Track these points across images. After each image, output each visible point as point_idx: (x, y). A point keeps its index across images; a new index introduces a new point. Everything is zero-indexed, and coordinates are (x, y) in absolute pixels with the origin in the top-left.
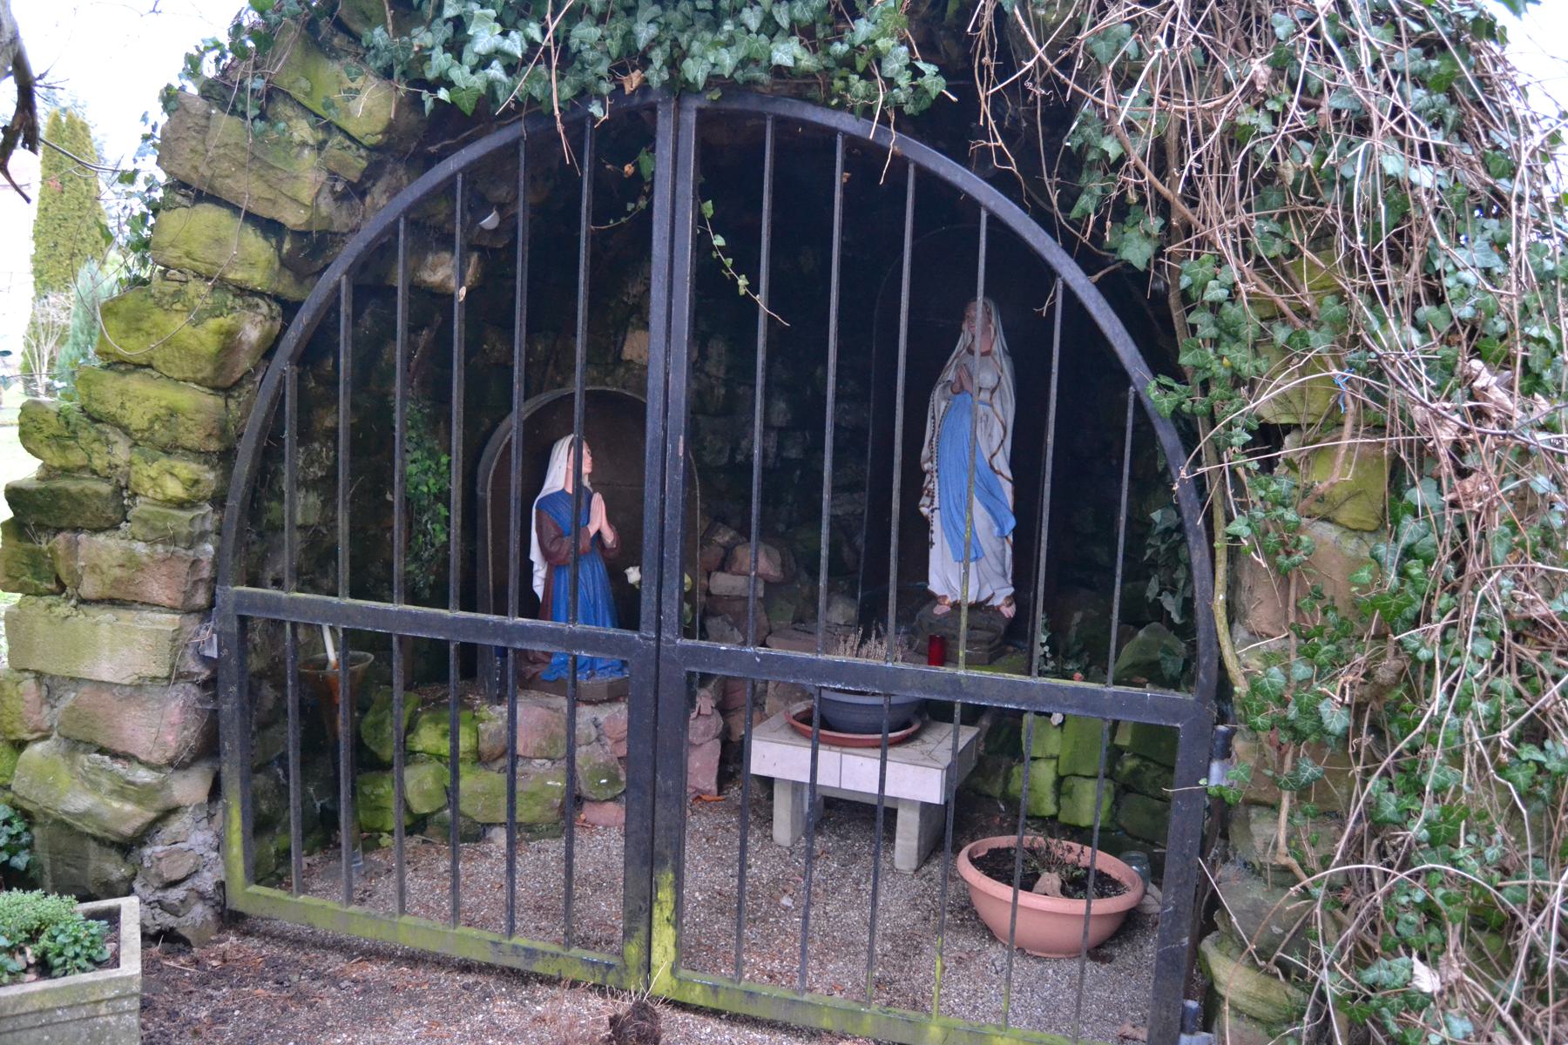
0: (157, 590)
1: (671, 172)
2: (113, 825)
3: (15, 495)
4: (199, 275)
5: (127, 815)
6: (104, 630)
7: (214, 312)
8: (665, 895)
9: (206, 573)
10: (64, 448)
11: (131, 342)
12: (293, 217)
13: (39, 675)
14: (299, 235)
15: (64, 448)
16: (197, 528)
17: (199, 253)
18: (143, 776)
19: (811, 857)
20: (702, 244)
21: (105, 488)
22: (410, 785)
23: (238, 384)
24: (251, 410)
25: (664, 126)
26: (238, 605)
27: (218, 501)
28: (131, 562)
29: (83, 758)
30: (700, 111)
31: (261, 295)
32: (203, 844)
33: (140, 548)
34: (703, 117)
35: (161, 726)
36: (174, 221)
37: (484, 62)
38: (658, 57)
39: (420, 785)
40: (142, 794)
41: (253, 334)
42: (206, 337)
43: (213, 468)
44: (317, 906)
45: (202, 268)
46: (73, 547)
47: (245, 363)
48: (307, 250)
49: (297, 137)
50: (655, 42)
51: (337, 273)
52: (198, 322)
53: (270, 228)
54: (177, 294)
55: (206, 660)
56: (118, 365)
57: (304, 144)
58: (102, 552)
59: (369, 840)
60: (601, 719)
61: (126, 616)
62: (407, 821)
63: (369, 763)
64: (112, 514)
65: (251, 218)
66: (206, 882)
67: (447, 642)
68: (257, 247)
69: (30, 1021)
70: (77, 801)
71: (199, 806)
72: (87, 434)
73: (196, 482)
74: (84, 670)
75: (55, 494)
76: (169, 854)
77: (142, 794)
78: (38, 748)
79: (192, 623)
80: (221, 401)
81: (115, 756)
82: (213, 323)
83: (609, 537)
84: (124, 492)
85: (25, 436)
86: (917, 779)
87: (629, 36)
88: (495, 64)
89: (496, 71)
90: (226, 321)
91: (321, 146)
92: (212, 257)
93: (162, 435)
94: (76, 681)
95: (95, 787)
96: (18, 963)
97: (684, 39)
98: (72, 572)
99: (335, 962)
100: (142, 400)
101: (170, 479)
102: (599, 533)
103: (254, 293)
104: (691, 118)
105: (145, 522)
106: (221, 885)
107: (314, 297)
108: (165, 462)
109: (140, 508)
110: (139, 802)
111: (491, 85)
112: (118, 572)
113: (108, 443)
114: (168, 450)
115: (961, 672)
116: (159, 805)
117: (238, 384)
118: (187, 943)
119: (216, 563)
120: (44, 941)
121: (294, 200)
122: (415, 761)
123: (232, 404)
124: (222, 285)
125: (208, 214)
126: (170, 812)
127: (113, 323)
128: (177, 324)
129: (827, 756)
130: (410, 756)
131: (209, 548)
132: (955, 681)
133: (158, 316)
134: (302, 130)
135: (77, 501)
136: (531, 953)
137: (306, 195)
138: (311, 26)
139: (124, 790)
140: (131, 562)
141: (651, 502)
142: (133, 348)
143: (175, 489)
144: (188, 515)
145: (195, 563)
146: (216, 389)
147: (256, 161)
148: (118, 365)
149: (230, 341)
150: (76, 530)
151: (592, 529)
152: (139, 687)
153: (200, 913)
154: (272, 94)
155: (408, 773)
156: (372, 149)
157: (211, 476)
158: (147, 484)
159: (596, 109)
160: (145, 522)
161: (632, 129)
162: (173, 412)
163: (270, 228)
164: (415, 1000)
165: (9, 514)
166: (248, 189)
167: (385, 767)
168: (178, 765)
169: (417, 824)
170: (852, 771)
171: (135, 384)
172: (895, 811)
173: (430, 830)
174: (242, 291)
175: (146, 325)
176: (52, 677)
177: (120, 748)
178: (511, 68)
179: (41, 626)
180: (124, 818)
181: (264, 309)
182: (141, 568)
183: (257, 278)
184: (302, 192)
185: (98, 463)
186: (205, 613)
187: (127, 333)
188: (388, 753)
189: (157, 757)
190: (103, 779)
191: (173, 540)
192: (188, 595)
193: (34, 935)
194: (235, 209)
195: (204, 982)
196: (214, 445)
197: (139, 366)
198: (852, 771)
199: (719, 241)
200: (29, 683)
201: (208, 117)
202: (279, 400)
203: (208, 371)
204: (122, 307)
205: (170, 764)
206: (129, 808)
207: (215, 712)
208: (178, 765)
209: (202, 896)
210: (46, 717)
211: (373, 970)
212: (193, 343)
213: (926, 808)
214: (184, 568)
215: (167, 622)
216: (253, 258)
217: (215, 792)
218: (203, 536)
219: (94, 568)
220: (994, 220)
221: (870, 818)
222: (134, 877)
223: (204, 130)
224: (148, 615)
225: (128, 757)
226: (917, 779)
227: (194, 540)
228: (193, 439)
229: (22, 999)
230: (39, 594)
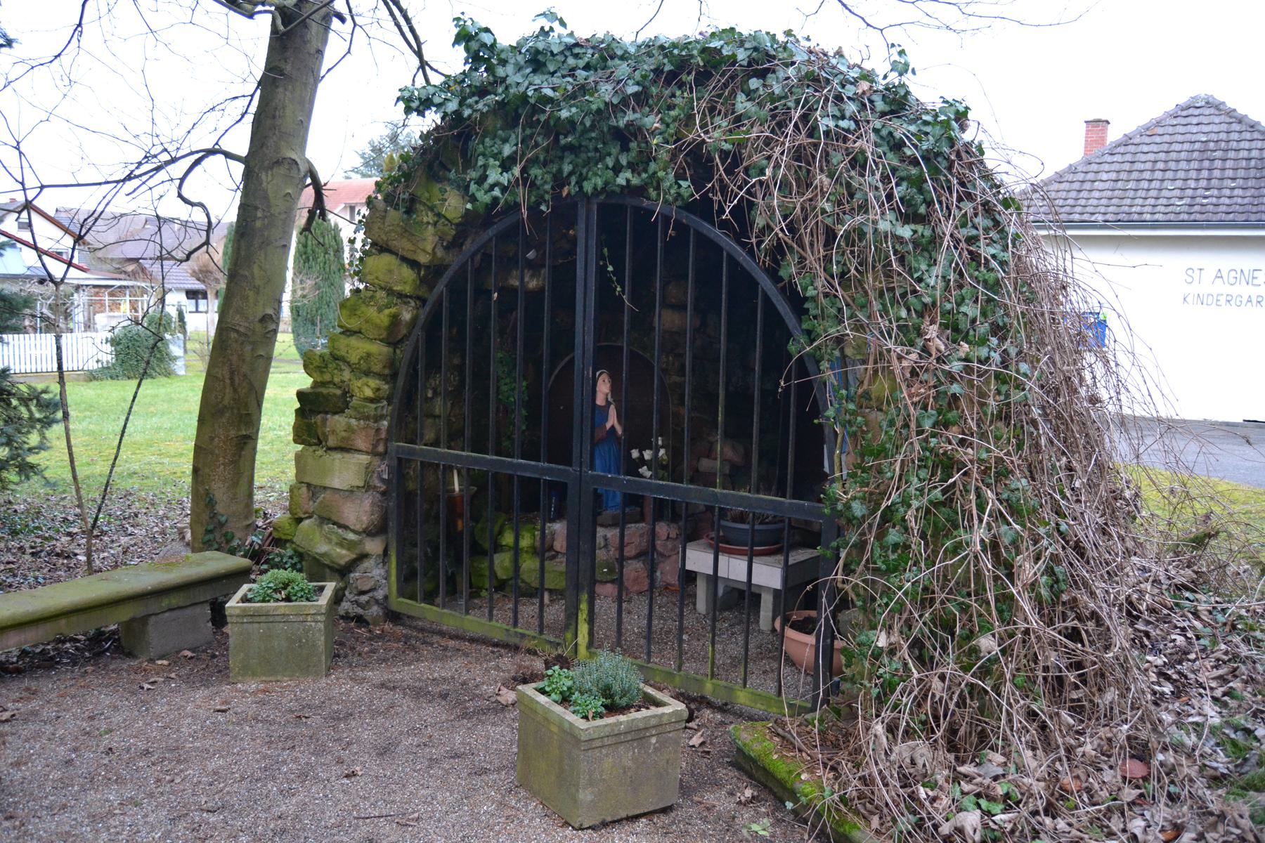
0: (361, 443)
1: (584, 233)
2: (337, 560)
3: (301, 395)
4: (381, 288)
5: (343, 555)
6: (337, 463)
7: (388, 306)
8: (584, 606)
9: (383, 436)
10: (322, 372)
11: (352, 321)
12: (423, 259)
13: (309, 485)
14: (427, 267)
15: (322, 372)
16: (379, 412)
17: (381, 277)
18: (351, 536)
19: (714, 620)
20: (602, 270)
21: (338, 392)
22: (497, 562)
23: (401, 341)
24: (403, 354)
25: (582, 212)
26: (397, 452)
27: (389, 400)
28: (349, 429)
29: (325, 527)
30: (599, 204)
31: (411, 297)
32: (378, 575)
33: (353, 421)
34: (601, 207)
35: (359, 513)
36: (370, 261)
37: (492, 187)
38: (573, 180)
39: (502, 562)
40: (350, 545)
41: (407, 316)
42: (383, 318)
43: (387, 383)
44: (429, 612)
45: (383, 284)
46: (324, 421)
47: (404, 331)
48: (430, 274)
49: (425, 219)
50: (571, 174)
51: (441, 287)
52: (380, 310)
53: (414, 264)
54: (372, 297)
55: (383, 480)
56: (348, 332)
57: (428, 223)
58: (338, 423)
59: (475, 592)
60: (609, 535)
61: (347, 456)
62: (495, 583)
63: (478, 551)
64: (341, 404)
65: (404, 259)
66: (380, 594)
67: (487, 472)
68: (407, 273)
69: (278, 619)
70: (322, 548)
71: (378, 556)
72: (332, 366)
73: (378, 389)
74: (329, 482)
75: (318, 395)
76: (362, 578)
77: (350, 545)
78: (307, 522)
79: (377, 461)
80: (391, 350)
81: (340, 526)
82: (387, 311)
83: (619, 430)
84: (347, 394)
85: (306, 367)
86: (769, 575)
87: (560, 170)
88: (497, 189)
89: (497, 192)
90: (393, 310)
91: (435, 224)
92: (387, 279)
93: (364, 366)
94: (325, 488)
95: (330, 541)
96: (278, 596)
97: (584, 171)
98: (324, 434)
99: (436, 638)
100: (357, 349)
101: (366, 388)
102: (613, 427)
103: (406, 296)
104: (595, 207)
105: (355, 409)
106: (386, 597)
107: (432, 298)
108: (365, 379)
109: (354, 402)
110: (348, 549)
111: (496, 200)
112: (344, 434)
113: (341, 370)
114: (367, 373)
115: (717, 490)
116: (357, 551)
117: (401, 341)
118: (368, 623)
119: (389, 430)
120: (289, 588)
121: (424, 251)
122: (502, 551)
123: (398, 351)
124: (390, 292)
125: (386, 259)
126: (363, 557)
127: (344, 311)
128: (372, 312)
129: (723, 559)
130: (498, 548)
131: (385, 423)
132: (715, 495)
133: (363, 308)
134: (430, 218)
135: (326, 398)
136: (523, 636)
137: (429, 248)
138: (430, 167)
139: (342, 543)
140: (349, 429)
141: (577, 401)
142: (353, 324)
143: (368, 393)
144: (374, 406)
145: (378, 430)
146: (389, 344)
147: (406, 232)
148: (348, 332)
149: (395, 319)
150: (327, 413)
151: (608, 425)
152: (352, 492)
153: (375, 610)
154: (413, 200)
155: (496, 556)
156: (457, 225)
157: (386, 387)
158: (357, 390)
159: (543, 208)
160: (355, 409)
161: (565, 211)
162: (369, 355)
163: (414, 264)
164: (466, 655)
165: (298, 405)
166: (404, 245)
167: (484, 553)
168: (369, 533)
169: (501, 586)
170: (734, 568)
171: (353, 341)
172: (759, 596)
173: (508, 589)
174: (401, 295)
175: (358, 313)
176: (316, 487)
177: (341, 522)
178: (504, 189)
179: (310, 460)
180: (342, 557)
181: (413, 304)
182: (353, 431)
183: (407, 289)
184: (427, 245)
185: (336, 380)
186: (383, 455)
187: (350, 317)
188: (487, 545)
189: (358, 527)
190: (333, 537)
191: (367, 418)
192: (375, 446)
193: (286, 586)
194: (396, 254)
195: (371, 639)
196: (387, 371)
197: (355, 332)
198: (734, 568)
199: (610, 268)
200: (304, 489)
201: (386, 211)
202: (416, 349)
203: (384, 335)
204: (348, 304)
205: (364, 531)
206: (344, 552)
207: (387, 509)
208: (369, 533)
209: (377, 602)
210: (311, 507)
211: (452, 643)
212: (378, 321)
213: (775, 591)
214: (372, 432)
215: (365, 459)
216: (405, 279)
217: (386, 552)
218: (382, 417)
219: (333, 432)
220: (730, 257)
221: (743, 599)
222: (345, 588)
223: (384, 218)
224: (357, 456)
225: (345, 527)
226: (769, 575)
227: (377, 419)
228: (377, 368)
229: (276, 608)
230: (310, 445)
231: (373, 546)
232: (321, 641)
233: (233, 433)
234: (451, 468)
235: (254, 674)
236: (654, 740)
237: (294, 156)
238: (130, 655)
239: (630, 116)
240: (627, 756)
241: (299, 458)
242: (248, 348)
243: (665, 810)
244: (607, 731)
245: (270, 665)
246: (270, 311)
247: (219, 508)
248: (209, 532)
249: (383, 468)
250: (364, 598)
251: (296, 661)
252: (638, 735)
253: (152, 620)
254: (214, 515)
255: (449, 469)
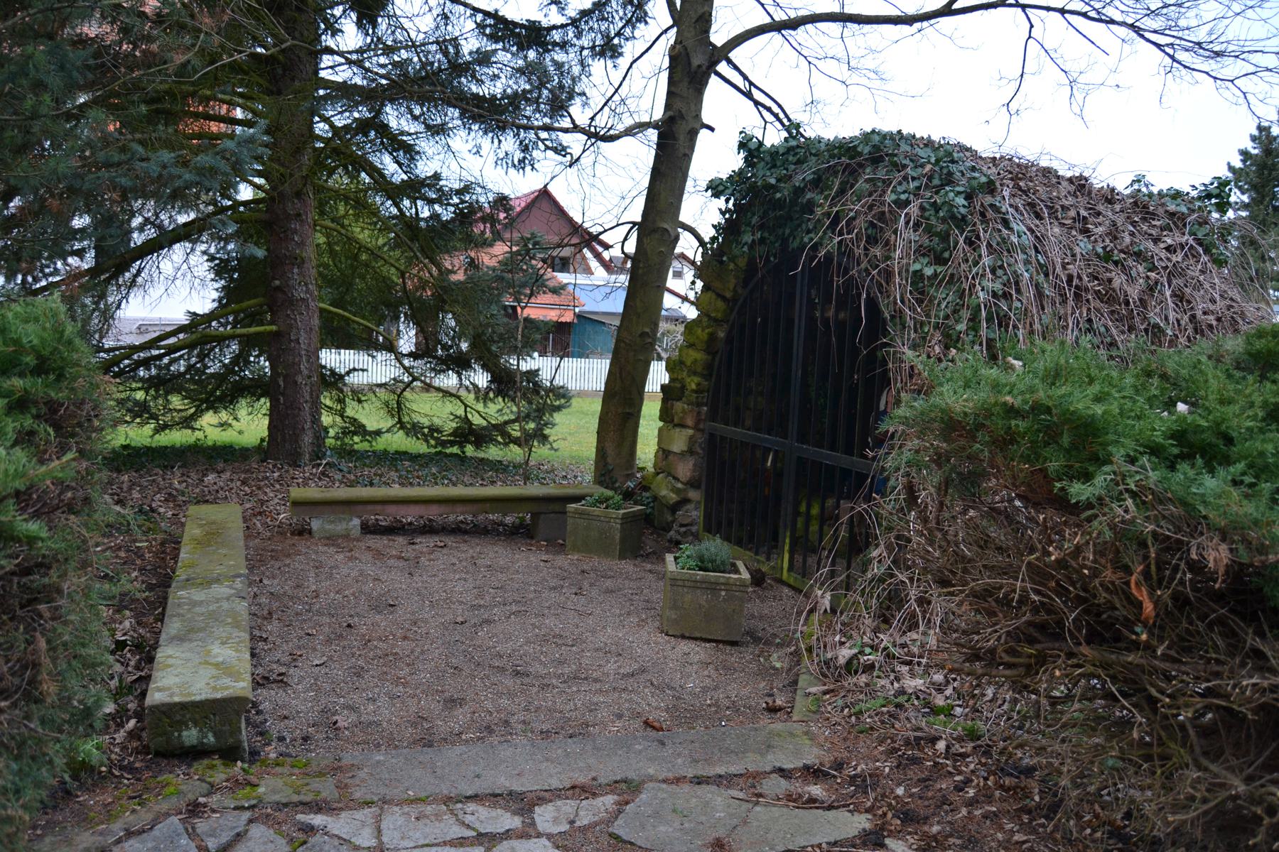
12: (728, 295)
18: (680, 485)
28: (684, 411)
77: (677, 491)
79: (699, 435)
114: (695, 373)
137: (731, 287)
143: (694, 386)
145: (699, 413)
146: (709, 353)
163: (723, 298)
174: (715, 320)
186: (702, 431)
189: (683, 480)
215: (691, 432)
231: (694, 495)
232: (618, 537)
233: (620, 411)
234: (770, 449)
235: (579, 551)
236: (723, 593)
237: (666, 226)
238: (532, 538)
239: (809, 195)
240: (703, 598)
241: (660, 430)
242: (631, 354)
243: (733, 644)
244: (687, 577)
245: (586, 548)
246: (647, 330)
247: (609, 460)
248: (603, 475)
249: (701, 438)
250: (683, 529)
251: (602, 548)
252: (713, 587)
253: (542, 516)
254: (606, 464)
255: (767, 450)
